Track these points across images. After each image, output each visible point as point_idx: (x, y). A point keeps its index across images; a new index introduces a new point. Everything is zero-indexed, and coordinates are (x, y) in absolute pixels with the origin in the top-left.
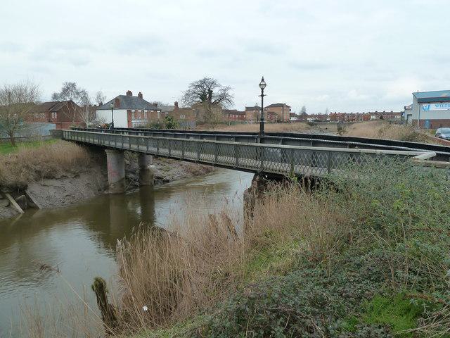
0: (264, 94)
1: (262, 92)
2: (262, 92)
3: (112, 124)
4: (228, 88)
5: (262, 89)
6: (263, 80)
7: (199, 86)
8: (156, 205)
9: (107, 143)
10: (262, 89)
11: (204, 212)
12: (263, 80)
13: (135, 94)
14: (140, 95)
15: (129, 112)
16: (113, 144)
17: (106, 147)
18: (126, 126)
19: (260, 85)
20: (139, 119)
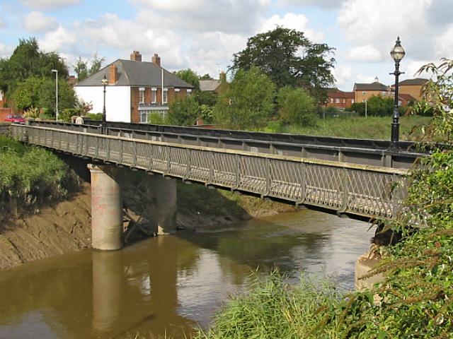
0: (400, 70)
1: (397, 66)
2: (397, 66)
3: (104, 116)
4: (323, 48)
5: (397, 62)
6: (398, 44)
7: (265, 44)
8: (113, 181)
9: (92, 153)
10: (397, 62)
11: (133, 105)
12: (398, 44)
13: (147, 58)
14: (157, 59)
15: (135, 91)
16: (103, 155)
17: (90, 160)
18: (126, 119)
19: (393, 53)
20: (152, 105)
